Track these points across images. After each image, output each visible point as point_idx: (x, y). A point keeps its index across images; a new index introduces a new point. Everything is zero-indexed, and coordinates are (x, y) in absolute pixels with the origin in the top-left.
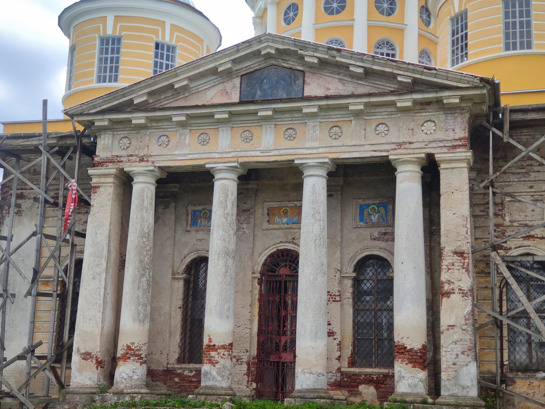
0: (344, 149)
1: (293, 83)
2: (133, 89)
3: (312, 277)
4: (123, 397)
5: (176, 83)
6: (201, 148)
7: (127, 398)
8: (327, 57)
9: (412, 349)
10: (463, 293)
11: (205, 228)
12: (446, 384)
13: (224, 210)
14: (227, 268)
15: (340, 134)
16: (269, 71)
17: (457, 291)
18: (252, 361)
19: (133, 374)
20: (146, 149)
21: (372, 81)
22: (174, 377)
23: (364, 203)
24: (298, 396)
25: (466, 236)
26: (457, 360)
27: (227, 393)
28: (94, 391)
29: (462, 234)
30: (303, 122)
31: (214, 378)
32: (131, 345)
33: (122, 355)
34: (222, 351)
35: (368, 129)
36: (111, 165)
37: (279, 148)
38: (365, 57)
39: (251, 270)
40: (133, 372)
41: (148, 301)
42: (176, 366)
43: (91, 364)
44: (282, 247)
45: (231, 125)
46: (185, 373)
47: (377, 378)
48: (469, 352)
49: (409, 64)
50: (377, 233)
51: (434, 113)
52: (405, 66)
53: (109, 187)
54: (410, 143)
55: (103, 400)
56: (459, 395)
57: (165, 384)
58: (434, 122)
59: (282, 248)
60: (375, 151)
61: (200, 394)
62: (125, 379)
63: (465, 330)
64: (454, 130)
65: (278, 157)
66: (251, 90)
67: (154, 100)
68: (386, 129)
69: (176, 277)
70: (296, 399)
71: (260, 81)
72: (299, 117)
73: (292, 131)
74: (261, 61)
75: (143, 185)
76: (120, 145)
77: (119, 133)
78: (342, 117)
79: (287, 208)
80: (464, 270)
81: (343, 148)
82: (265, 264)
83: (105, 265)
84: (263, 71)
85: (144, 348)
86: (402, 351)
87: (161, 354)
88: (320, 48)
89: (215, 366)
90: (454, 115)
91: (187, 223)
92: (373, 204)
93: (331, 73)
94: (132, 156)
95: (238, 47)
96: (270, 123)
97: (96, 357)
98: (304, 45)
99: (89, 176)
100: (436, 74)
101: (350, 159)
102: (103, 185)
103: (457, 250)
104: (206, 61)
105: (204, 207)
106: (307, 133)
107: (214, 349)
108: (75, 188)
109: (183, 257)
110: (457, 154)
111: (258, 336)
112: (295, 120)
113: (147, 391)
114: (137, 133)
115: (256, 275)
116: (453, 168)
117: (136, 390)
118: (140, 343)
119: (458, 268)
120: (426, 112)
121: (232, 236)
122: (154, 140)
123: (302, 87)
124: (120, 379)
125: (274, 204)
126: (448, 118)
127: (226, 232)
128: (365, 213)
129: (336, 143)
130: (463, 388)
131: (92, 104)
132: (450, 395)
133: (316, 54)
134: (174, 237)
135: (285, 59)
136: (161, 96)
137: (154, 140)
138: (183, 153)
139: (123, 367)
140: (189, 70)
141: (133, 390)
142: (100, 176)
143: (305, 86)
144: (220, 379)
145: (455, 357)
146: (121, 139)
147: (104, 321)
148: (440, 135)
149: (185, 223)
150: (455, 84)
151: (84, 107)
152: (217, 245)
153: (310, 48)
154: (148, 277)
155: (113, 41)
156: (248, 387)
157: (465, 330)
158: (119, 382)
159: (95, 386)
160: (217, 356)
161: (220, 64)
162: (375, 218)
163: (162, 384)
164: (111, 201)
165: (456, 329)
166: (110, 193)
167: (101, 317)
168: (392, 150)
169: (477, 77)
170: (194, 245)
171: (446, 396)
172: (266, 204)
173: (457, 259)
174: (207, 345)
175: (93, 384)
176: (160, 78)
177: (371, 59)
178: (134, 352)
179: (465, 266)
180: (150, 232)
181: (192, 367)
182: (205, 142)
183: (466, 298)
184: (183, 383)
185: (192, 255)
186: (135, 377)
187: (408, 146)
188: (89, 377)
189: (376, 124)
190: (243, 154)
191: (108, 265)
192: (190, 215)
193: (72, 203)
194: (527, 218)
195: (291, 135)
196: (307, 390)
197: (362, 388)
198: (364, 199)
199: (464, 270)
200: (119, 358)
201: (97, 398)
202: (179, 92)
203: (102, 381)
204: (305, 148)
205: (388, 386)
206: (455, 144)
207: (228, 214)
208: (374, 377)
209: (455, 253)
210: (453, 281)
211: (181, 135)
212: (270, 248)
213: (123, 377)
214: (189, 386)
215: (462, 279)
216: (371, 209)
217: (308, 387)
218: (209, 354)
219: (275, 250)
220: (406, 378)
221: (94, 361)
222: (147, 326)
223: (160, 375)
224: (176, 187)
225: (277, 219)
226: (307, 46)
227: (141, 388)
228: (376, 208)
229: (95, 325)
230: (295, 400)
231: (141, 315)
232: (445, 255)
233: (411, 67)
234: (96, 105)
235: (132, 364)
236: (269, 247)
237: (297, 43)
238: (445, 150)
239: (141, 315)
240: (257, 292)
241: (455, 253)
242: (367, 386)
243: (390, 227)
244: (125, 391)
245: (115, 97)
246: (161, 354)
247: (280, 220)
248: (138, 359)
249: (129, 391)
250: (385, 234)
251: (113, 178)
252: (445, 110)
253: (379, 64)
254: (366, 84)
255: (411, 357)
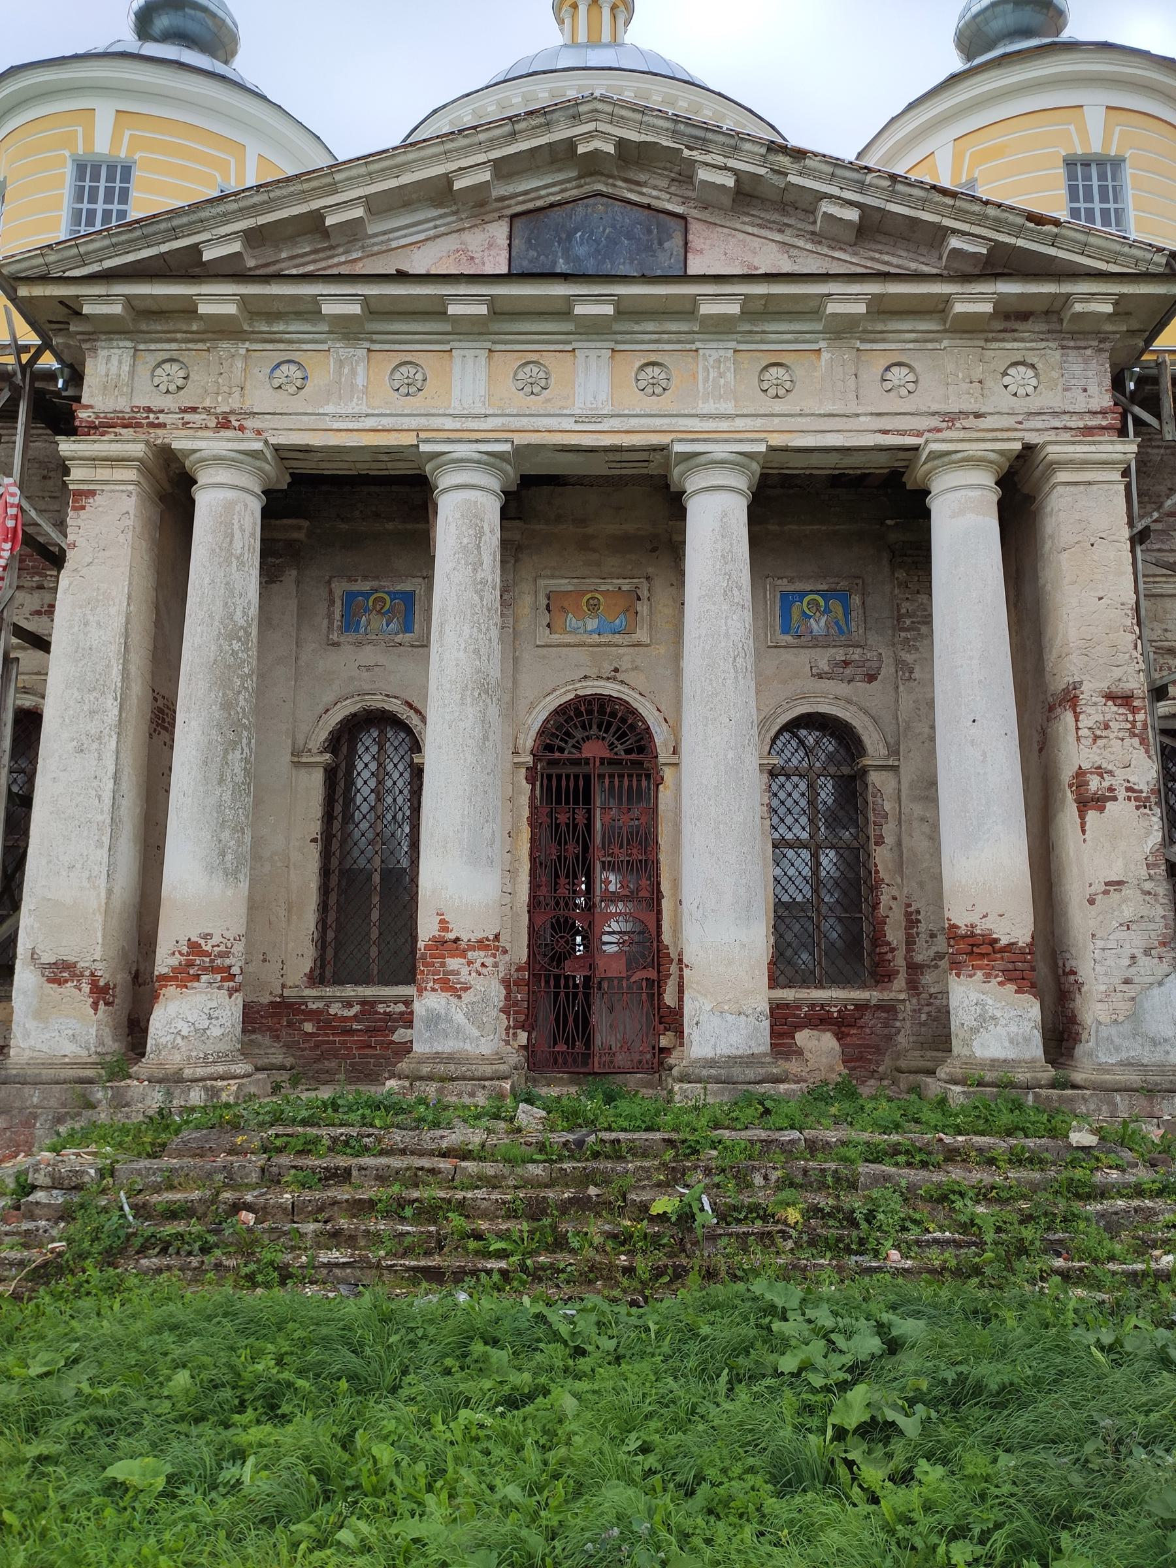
0: (801, 423)
1: (655, 246)
2: (203, 214)
3: (730, 755)
4: (183, 1092)
5: (332, 213)
6: (403, 404)
7: (196, 1097)
8: (762, 171)
9: (1013, 944)
10: (1136, 799)
11: (380, 637)
12: (1110, 1034)
13: (475, 570)
14: (486, 727)
15: (788, 385)
16: (590, 210)
17: (1121, 794)
18: (515, 975)
19: (208, 1022)
20: (237, 395)
21: (872, 254)
22: (302, 1022)
23: (791, 588)
24: (710, 1077)
25: (1135, 654)
26: (1133, 970)
27: (497, 1071)
28: (89, 1073)
29: (1125, 650)
30: (688, 347)
31: (459, 1030)
32: (202, 942)
33: (174, 969)
34: (478, 956)
35: (863, 375)
36: (127, 433)
37: (626, 412)
38: (869, 178)
39: (511, 746)
40: (210, 1018)
41: (247, 817)
42: (307, 992)
43: (78, 996)
44: (590, 688)
45: (488, 345)
46: (332, 1011)
47: (839, 1011)
48: (1162, 950)
49: (987, 203)
50: (825, 661)
51: (1033, 345)
52: (976, 208)
53: (124, 496)
54: (978, 416)
55: (120, 1102)
56: (1145, 1061)
57: (277, 1038)
58: (1033, 366)
59: (589, 692)
60: (886, 432)
61: (421, 1078)
62: (183, 1037)
63: (1149, 893)
64: (1085, 390)
65: (623, 435)
66: (539, 255)
67: (260, 262)
68: (911, 377)
69: (304, 760)
70: (709, 1086)
71: (564, 236)
72: (679, 332)
73: (657, 370)
74: (569, 181)
75: (230, 494)
76: (156, 381)
77: (153, 346)
78: (796, 341)
79: (597, 595)
80: (1136, 741)
81: (799, 419)
82: (542, 732)
83: (116, 712)
84: (572, 209)
85: (239, 948)
86: (985, 949)
87: (264, 960)
88: (747, 146)
89: (460, 997)
90: (1082, 351)
91: (331, 622)
92: (812, 592)
93: (760, 226)
94: (194, 410)
95: (513, 123)
96: (599, 345)
97: (92, 974)
98: (700, 133)
99: (64, 459)
100: (1056, 235)
101: (816, 454)
102: (104, 487)
103: (1114, 689)
104: (423, 153)
105: (375, 584)
106: (700, 377)
107: (457, 949)
108: (16, 500)
109: (320, 709)
110: (1102, 448)
111: (529, 912)
112: (669, 342)
113: (249, 1068)
114: (208, 350)
115: (522, 760)
116: (1089, 483)
117: (221, 1069)
118: (227, 934)
119: (1121, 735)
120: (1015, 340)
121: (495, 643)
122: (260, 373)
123: (682, 258)
124: (170, 1038)
125: (563, 584)
126: (1070, 359)
127: (480, 631)
128: (795, 613)
129: (778, 407)
130: (1155, 1043)
131: (74, 251)
132: (1121, 1064)
133: (731, 163)
134: (297, 659)
135: (636, 178)
136: (281, 251)
137: (260, 373)
138: (350, 411)
139: (178, 1003)
140: (371, 177)
141: (210, 1070)
142: (95, 461)
143: (690, 256)
144: (477, 1033)
145: (1127, 962)
146: (159, 365)
147: (115, 871)
148: (1051, 399)
149: (326, 622)
150: (1102, 266)
151: (52, 258)
152: (457, 665)
153: (715, 142)
154: (246, 750)
155: (111, 169)
156: (507, 1043)
157: (1149, 893)
158: (165, 1046)
159: (90, 1060)
160: (465, 970)
161: (461, 169)
162: (818, 625)
163: (267, 1040)
164: (130, 533)
165: (1127, 891)
166: (127, 513)
167: (106, 860)
168: (929, 431)
169: (1164, 249)
170: (352, 679)
171: (1113, 1065)
172: (542, 582)
173: (1116, 713)
174: (434, 939)
175: (85, 1053)
176: (285, 192)
177: (886, 183)
178: (212, 961)
179: (1137, 732)
180: (250, 625)
181: (353, 994)
182: (412, 388)
183: (1147, 811)
184: (327, 1035)
185: (346, 706)
186: (216, 1032)
187: (971, 422)
188: (71, 1032)
189: (884, 363)
190: (524, 422)
191: (124, 715)
192: (338, 603)
193: (5, 541)
194: (1168, 635)
195: (655, 381)
196: (733, 1061)
197: (803, 1038)
198: (792, 578)
199: (1136, 741)
200: (164, 978)
201: (100, 1095)
202: (333, 243)
203: (109, 1041)
204: (697, 415)
205: (868, 1031)
206: (1090, 423)
207: (484, 582)
208: (833, 1009)
209: (1110, 697)
210: (1110, 767)
211: (341, 363)
212: (558, 693)
213: (178, 1033)
214: (344, 1043)
215: (1133, 763)
216: (808, 604)
217: (734, 1052)
218: (443, 965)
219: (571, 696)
220: (1002, 1022)
221: (86, 988)
222: (244, 886)
223: (262, 1017)
224: (300, 528)
225: (572, 621)
226: (710, 136)
227: (233, 1062)
228: (822, 603)
229: (85, 884)
230: (705, 1088)
231: (229, 857)
232: (1083, 702)
233: (992, 211)
234: (87, 253)
235: (207, 993)
236: (554, 690)
237: (682, 127)
238: (1066, 436)
239: (229, 857)
240: (524, 800)
241: (1110, 697)
242: (815, 1033)
243: (858, 646)
244: (188, 1073)
245: (145, 237)
246: (264, 960)
247: (580, 623)
248: (223, 980)
249: (200, 1072)
250: (846, 663)
251: (135, 471)
252: (1063, 339)
253: (905, 200)
254: (853, 260)
255: (1010, 966)
